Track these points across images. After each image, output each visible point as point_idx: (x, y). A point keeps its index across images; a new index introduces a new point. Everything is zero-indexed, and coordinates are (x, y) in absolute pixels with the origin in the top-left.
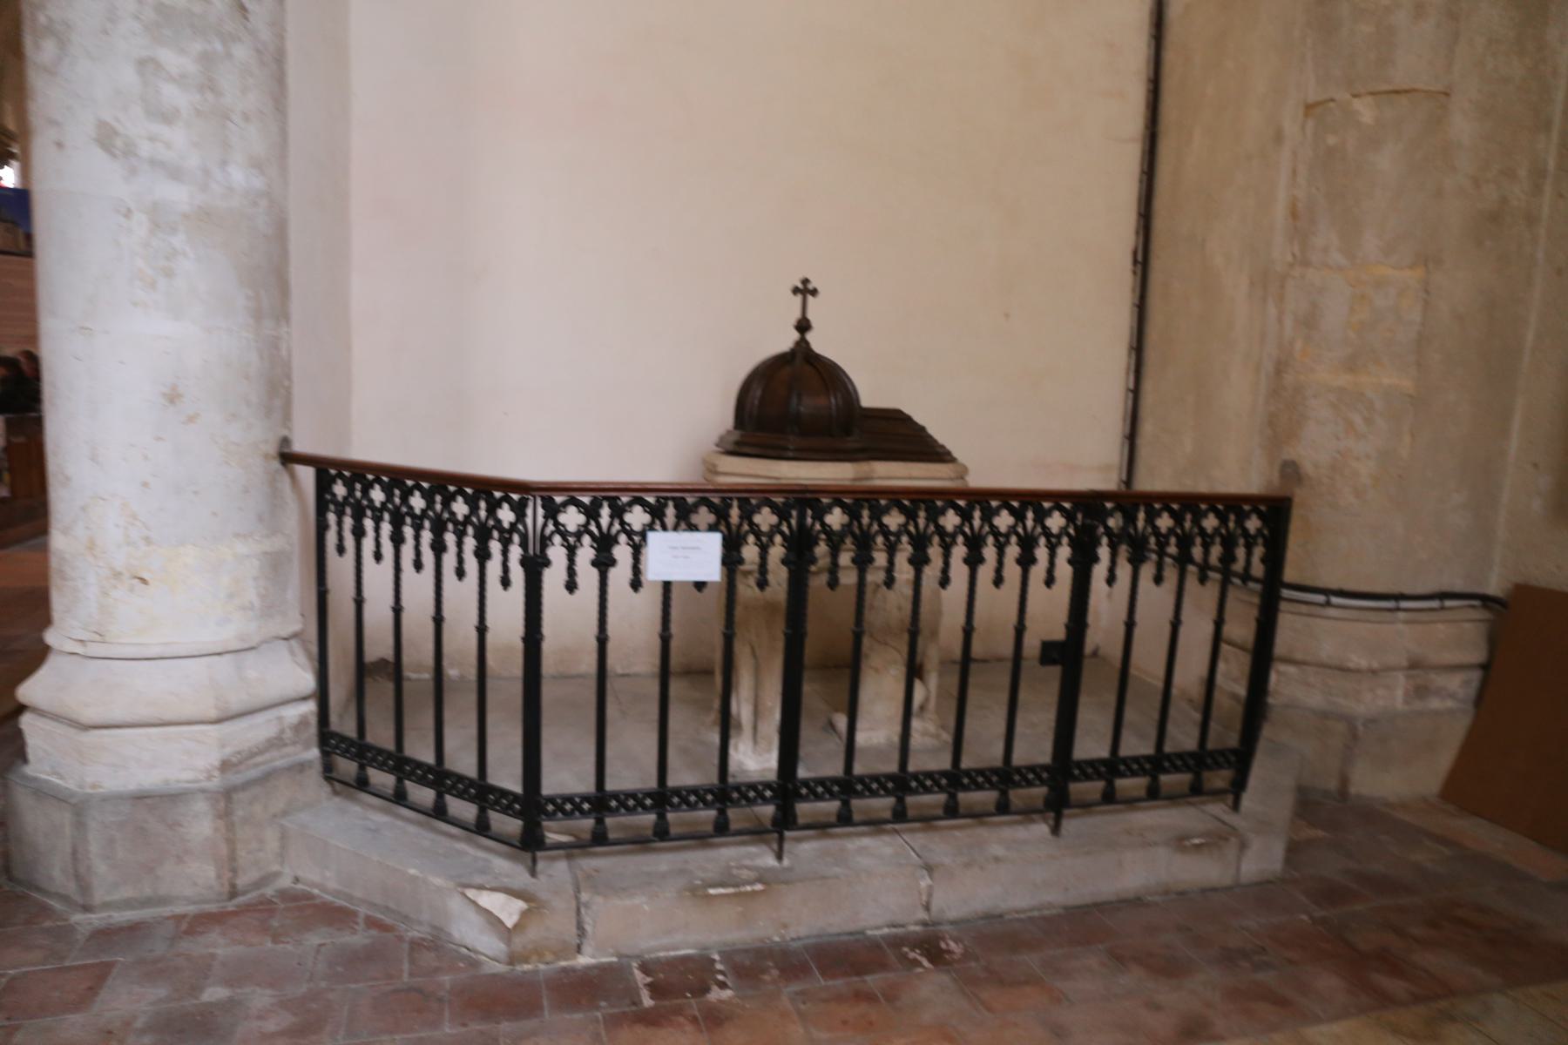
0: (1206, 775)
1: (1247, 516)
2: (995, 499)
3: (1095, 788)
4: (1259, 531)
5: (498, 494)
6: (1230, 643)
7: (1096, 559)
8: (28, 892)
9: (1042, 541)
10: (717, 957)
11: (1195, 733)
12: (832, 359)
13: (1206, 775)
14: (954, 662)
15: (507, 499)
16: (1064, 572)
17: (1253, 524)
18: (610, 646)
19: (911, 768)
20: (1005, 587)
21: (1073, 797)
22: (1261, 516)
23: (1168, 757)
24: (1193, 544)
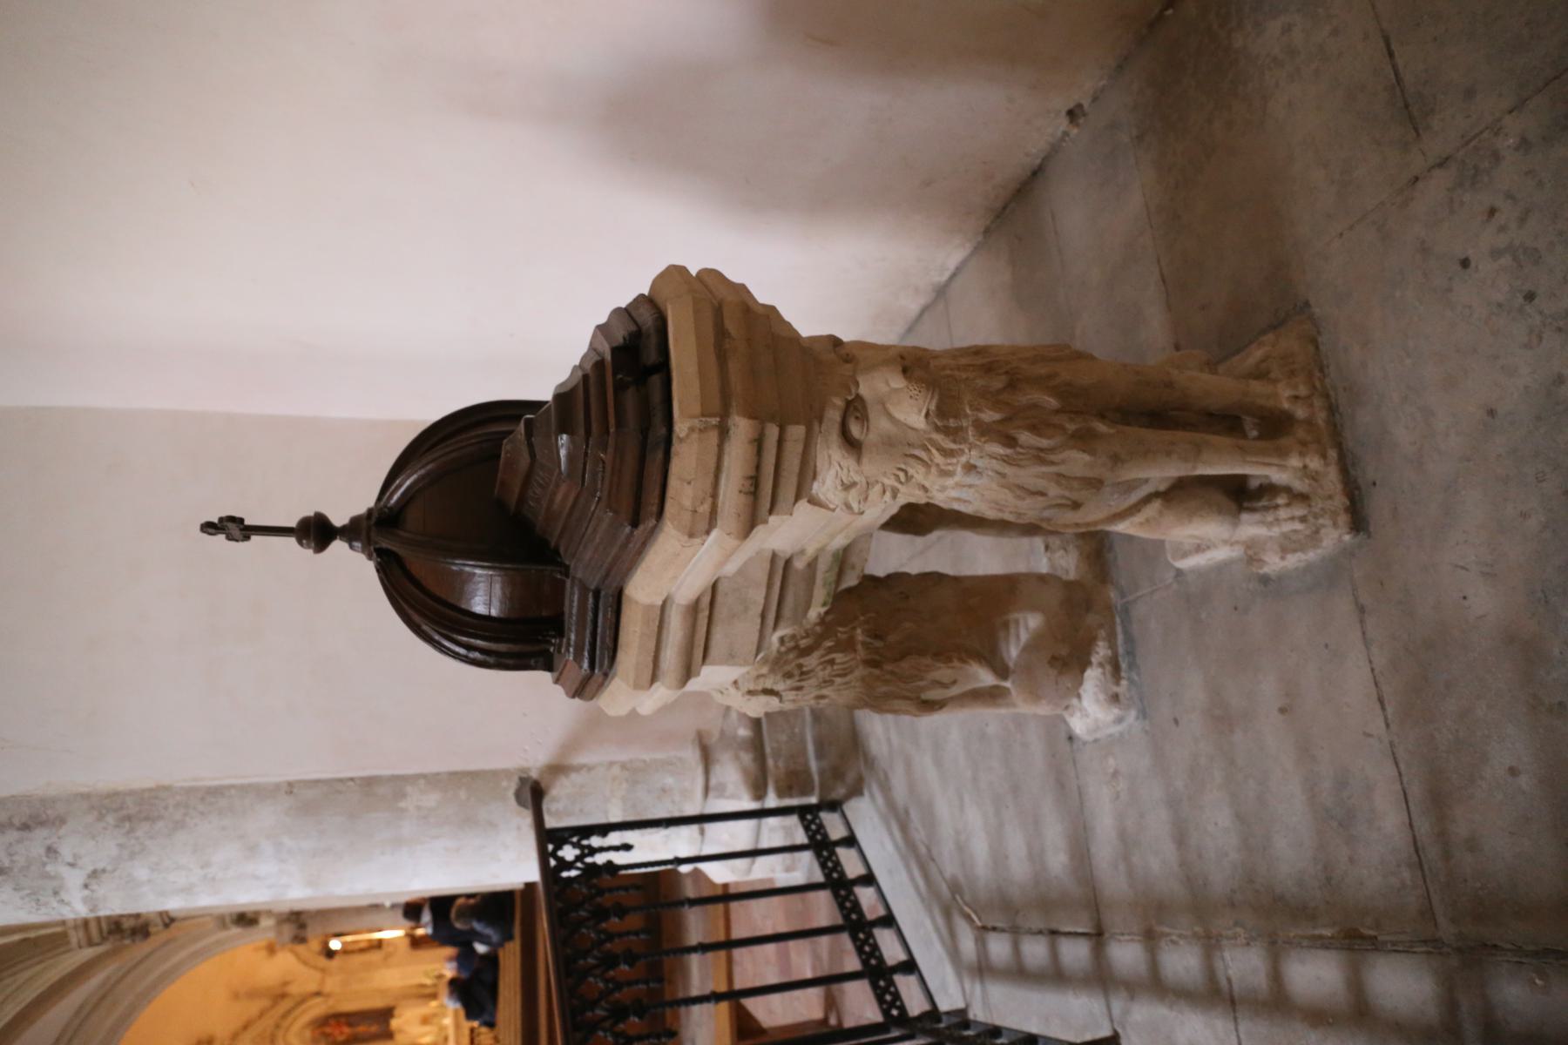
0: (870, 916)
1: (561, 860)
2: (547, 848)
3: (907, 986)
4: (575, 845)
5: (553, 862)
6: (701, 850)
7: (610, 863)
8: (816, 778)
9: (589, 860)
10: (859, 647)
11: (812, 896)
12: (402, 623)
13: (870, 916)
14: (702, 832)
15: (554, 854)
16: (614, 838)
17: (569, 853)
18: (708, 940)
19: (840, 921)
20: (630, 842)
21: (926, 1007)
22: (559, 847)
23: (828, 876)
24: (594, 864)
